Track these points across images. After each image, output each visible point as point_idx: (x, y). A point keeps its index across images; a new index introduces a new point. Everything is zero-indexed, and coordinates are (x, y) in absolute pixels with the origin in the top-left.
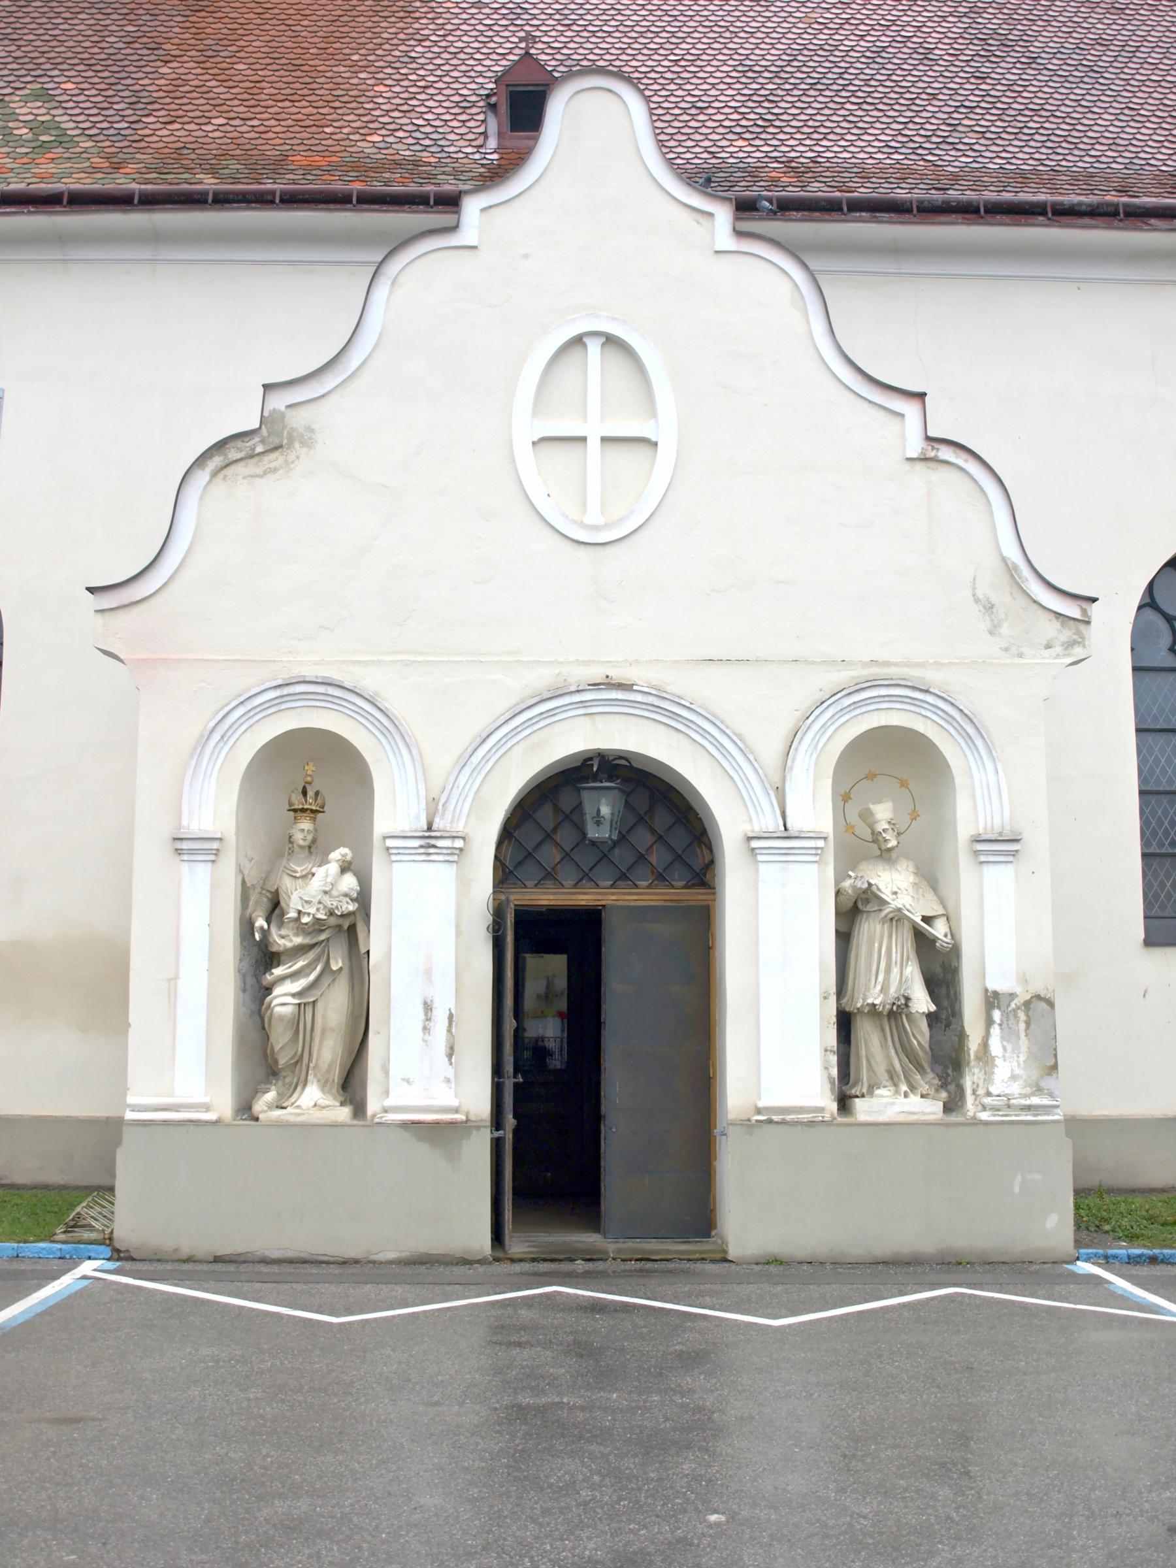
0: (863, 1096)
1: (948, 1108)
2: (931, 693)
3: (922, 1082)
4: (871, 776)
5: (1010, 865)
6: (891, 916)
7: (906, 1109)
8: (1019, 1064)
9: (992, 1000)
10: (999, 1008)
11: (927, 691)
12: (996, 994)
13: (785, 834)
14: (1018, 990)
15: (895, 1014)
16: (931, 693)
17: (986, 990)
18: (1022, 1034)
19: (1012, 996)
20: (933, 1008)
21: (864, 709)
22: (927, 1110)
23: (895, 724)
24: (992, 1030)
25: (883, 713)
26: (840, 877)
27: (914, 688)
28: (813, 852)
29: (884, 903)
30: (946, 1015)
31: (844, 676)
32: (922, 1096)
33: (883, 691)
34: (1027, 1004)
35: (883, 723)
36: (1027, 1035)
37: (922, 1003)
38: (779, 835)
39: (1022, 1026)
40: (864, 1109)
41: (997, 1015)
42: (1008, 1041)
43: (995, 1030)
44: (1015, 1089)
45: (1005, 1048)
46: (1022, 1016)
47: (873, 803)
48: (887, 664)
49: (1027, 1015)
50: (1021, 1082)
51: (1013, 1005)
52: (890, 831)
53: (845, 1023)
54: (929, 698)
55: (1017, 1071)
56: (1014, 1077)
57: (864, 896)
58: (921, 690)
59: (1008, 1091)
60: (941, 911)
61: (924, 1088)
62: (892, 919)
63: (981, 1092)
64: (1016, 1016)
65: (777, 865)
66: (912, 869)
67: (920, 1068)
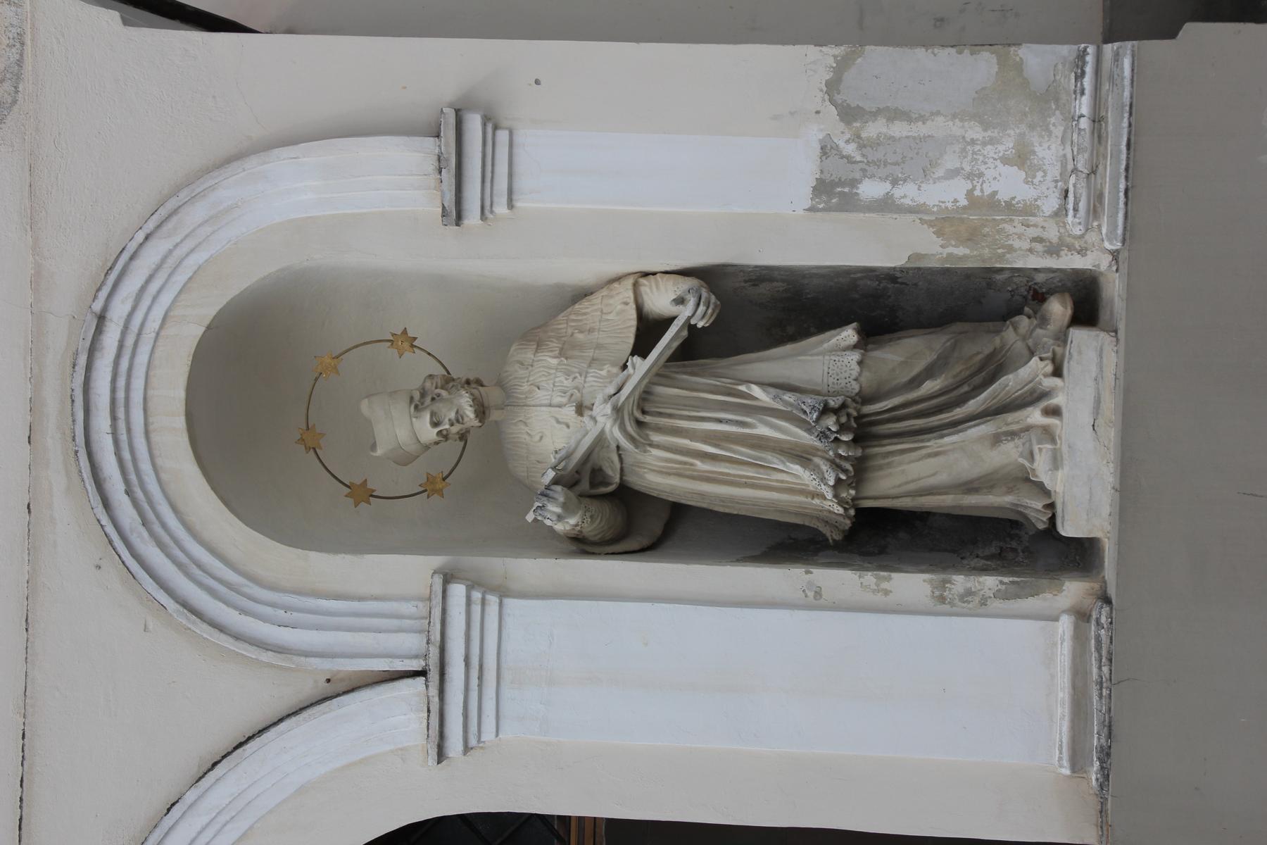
0: (1051, 506)
1: (1087, 305)
2: (105, 309)
3: (1024, 372)
4: (311, 442)
5: (518, 139)
6: (630, 428)
7: (1086, 418)
8: (992, 141)
9: (832, 193)
10: (854, 183)
11: (101, 318)
12: (823, 188)
13: (434, 675)
14: (814, 134)
15: (860, 428)
16: (105, 309)
17: (812, 209)
18: (921, 129)
19: (826, 150)
20: (849, 335)
21: (146, 466)
22: (1094, 369)
23: (182, 394)
24: (907, 201)
25: (156, 423)
26: (544, 542)
27: (92, 351)
28: (476, 609)
29: (600, 440)
30: (874, 306)
31: (67, 513)
32: (1057, 372)
33: (102, 422)
34: (849, 114)
35: (180, 422)
36: (922, 119)
37: (832, 360)
38: (434, 691)
39: (899, 129)
40: (1082, 492)
41: (871, 189)
42: (933, 164)
43: (908, 193)
44: (1049, 152)
45: (953, 173)
46: (873, 129)
47: (374, 447)
48: (35, 406)
49: (875, 114)
50: (1034, 138)
51: (850, 149)
52: (438, 406)
53: (880, 535)
54: (119, 310)
55: (1007, 146)
56: (1022, 158)
57: (585, 486)
58: (99, 330)
59: (1054, 172)
60: (625, 292)
61: (1035, 370)
62: (640, 424)
63: (1052, 234)
64: (875, 144)
65: (506, 692)
66: (529, 355)
67: (994, 368)
